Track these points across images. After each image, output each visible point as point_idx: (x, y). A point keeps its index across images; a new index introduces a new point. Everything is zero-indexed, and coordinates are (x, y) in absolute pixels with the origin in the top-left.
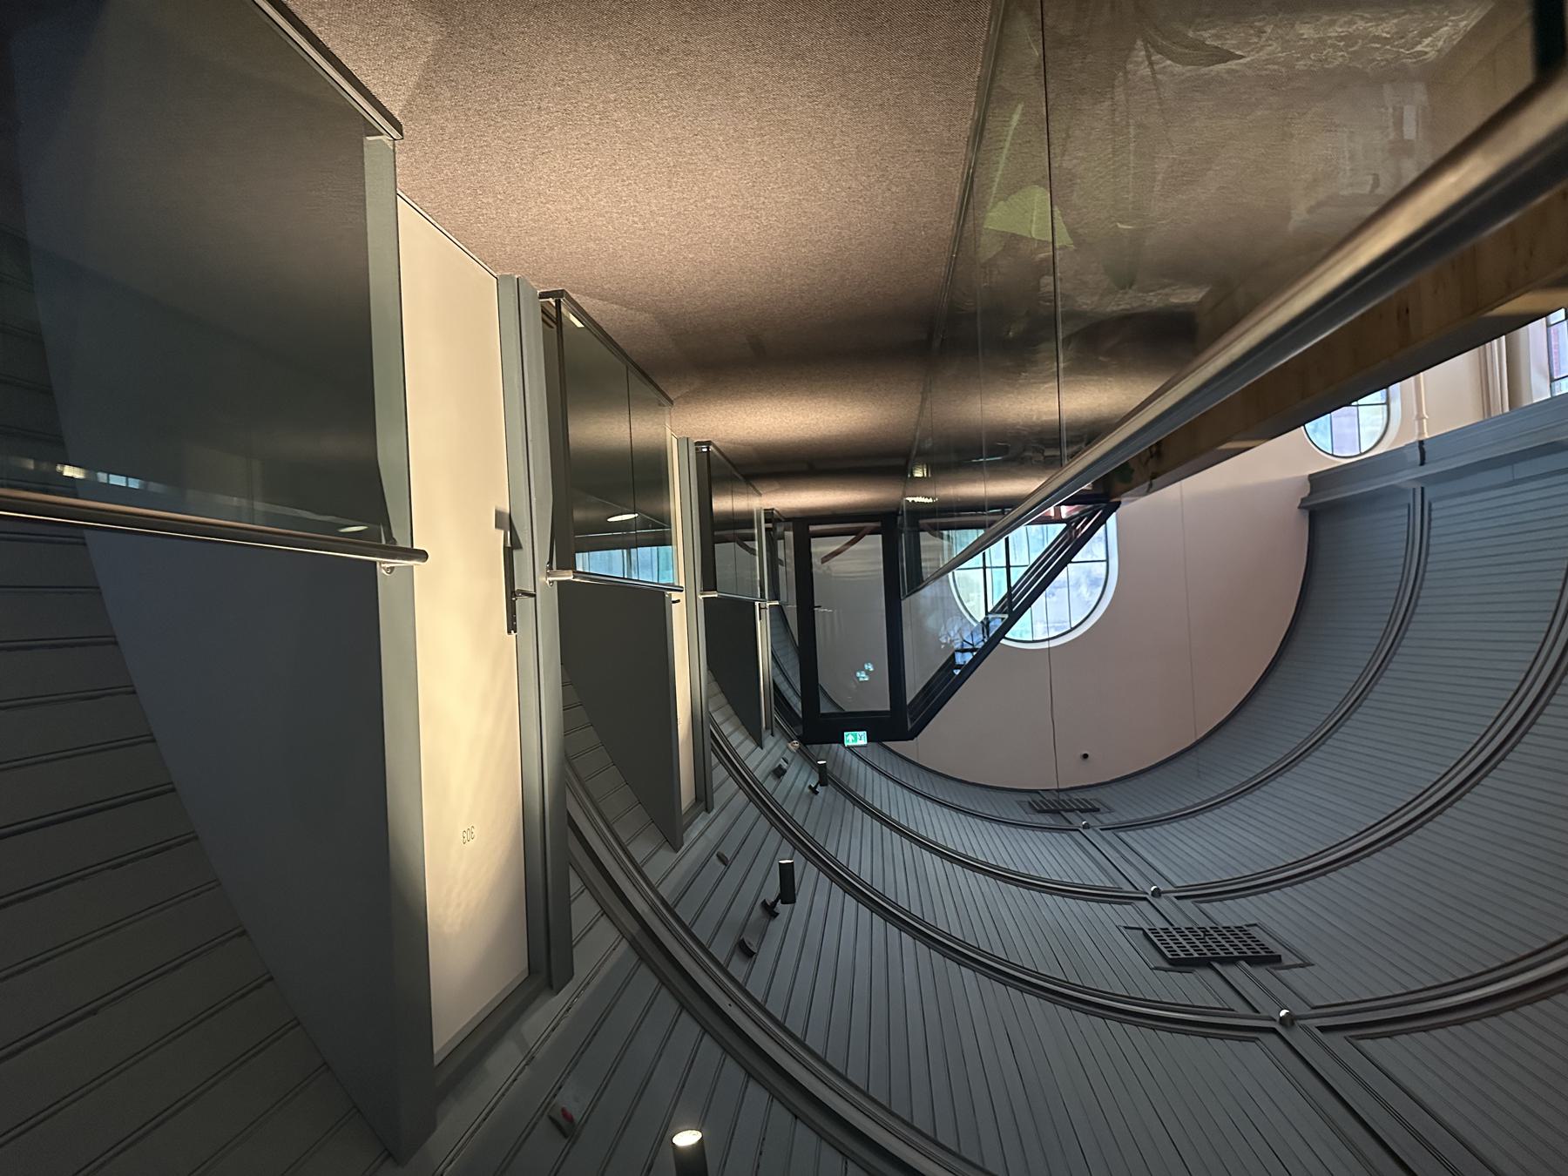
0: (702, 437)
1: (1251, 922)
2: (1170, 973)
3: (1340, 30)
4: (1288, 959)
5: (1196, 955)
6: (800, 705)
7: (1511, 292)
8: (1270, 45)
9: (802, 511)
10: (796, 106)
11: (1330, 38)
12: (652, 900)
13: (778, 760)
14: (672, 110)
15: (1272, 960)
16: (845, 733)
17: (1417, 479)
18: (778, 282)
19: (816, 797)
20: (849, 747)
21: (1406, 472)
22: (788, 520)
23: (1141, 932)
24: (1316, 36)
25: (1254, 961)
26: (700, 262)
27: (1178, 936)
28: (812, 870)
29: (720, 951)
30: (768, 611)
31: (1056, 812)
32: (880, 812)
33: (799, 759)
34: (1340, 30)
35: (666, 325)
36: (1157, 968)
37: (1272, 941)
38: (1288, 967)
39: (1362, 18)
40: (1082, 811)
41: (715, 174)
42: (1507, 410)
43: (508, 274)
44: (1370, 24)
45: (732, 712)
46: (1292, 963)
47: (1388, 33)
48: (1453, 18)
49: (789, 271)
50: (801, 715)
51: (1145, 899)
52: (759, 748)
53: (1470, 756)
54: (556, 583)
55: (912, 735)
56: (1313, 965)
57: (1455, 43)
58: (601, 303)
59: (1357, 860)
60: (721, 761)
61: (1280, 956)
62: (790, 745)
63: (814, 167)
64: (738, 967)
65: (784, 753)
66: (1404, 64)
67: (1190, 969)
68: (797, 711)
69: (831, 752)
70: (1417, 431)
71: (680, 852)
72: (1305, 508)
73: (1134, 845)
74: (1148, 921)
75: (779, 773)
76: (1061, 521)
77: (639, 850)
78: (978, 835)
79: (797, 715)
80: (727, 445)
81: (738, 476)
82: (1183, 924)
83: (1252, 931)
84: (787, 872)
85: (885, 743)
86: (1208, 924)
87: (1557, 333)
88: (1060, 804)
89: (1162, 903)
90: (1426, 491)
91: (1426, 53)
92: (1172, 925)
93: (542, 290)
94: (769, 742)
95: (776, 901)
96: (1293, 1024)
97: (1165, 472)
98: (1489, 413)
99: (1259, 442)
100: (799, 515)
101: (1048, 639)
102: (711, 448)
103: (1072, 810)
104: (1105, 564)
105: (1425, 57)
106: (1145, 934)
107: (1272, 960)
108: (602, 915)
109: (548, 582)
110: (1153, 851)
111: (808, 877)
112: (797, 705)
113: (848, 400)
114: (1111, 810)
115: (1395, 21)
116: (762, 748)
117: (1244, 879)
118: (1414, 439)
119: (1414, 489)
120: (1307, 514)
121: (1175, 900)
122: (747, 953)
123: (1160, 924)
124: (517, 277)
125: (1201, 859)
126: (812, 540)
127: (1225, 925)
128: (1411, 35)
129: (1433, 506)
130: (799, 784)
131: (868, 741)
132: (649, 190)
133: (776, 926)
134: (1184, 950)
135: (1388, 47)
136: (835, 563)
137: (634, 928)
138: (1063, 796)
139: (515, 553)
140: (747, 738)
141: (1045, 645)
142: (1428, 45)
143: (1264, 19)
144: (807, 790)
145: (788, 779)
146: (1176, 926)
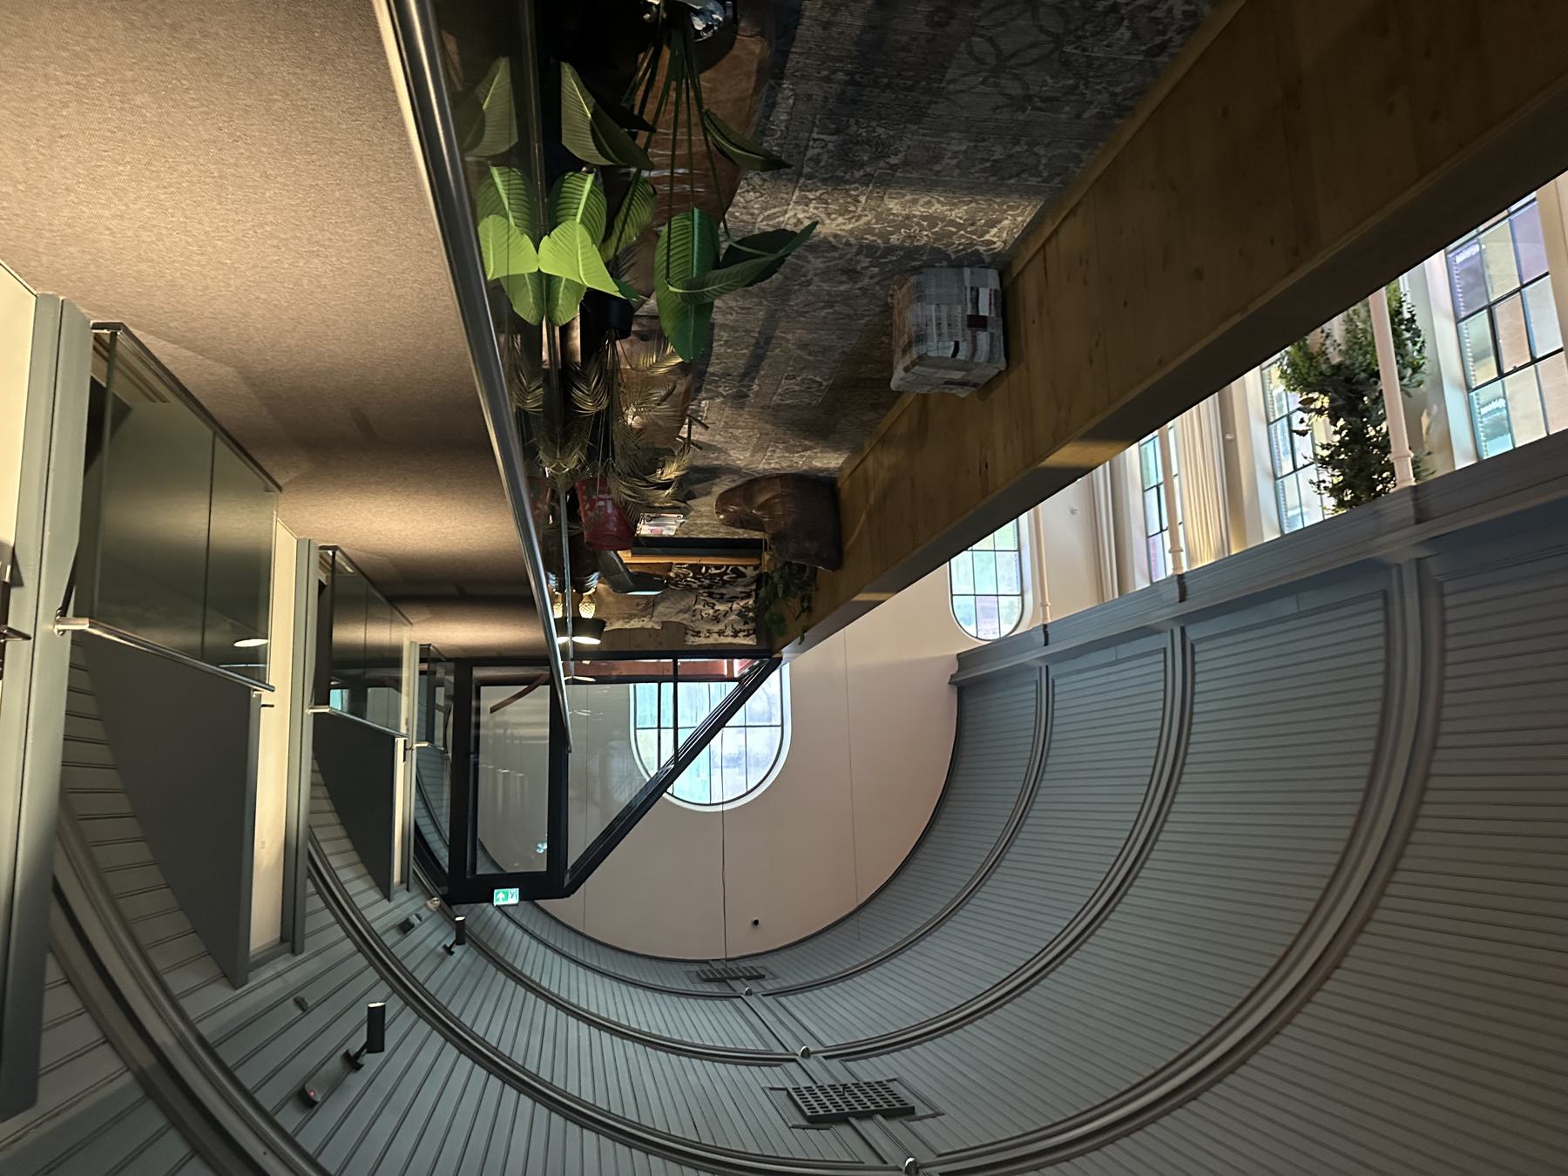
0: (327, 541)
1: (891, 1077)
2: (807, 1131)
3: (923, 210)
4: (921, 1110)
5: (834, 1111)
6: (447, 860)
7: (1057, 443)
8: (866, 215)
9: (465, 649)
10: (339, 123)
11: (915, 216)
12: (182, 1034)
13: (411, 914)
14: (202, 105)
15: (907, 1112)
16: (496, 891)
17: (1041, 658)
18: (368, 343)
19: (449, 957)
20: (498, 907)
21: (1034, 652)
22: (449, 660)
23: (785, 1092)
24: (904, 212)
25: (889, 1114)
26: (276, 306)
27: (819, 1094)
28: (409, 1016)
29: (269, 1098)
30: (415, 752)
31: (722, 980)
32: (558, 997)
33: (438, 918)
34: (923, 210)
35: (254, 385)
36: (794, 1127)
37: (908, 1094)
38: (920, 1119)
39: (939, 202)
40: (749, 978)
41: (267, 195)
42: (1117, 596)
43: (50, 293)
44: (945, 208)
45: (365, 871)
46: (924, 1114)
47: (960, 218)
48: (1010, 212)
49: (378, 331)
50: (447, 870)
51: (794, 1060)
52: (385, 901)
53: (1087, 908)
54: (68, 636)
55: (568, 892)
56: (943, 1114)
57: (1016, 236)
58: (170, 346)
59: (991, 1012)
60: (319, 892)
61: (913, 1108)
62: (429, 903)
63: (374, 202)
64: (290, 1118)
65: (421, 908)
66: (977, 251)
67: (826, 1125)
68: (443, 865)
69: (483, 917)
70: (1041, 616)
71: (238, 992)
72: (955, 683)
73: (792, 1009)
74: (793, 1080)
75: (406, 927)
76: (734, 680)
77: (178, 982)
78: (636, 1003)
79: (444, 871)
80: (359, 553)
81: (379, 596)
82: (826, 1081)
83: (891, 1086)
84: (376, 1020)
85: (539, 902)
86: (849, 1080)
87: (1154, 544)
88: (726, 972)
89: (810, 1064)
90: (1050, 668)
91: (995, 243)
92: (815, 1083)
93: (96, 321)
94: (401, 896)
95: (362, 1050)
96: (917, 1172)
97: (813, 626)
98: (1103, 600)
99: (888, 595)
100: (463, 655)
101: (723, 803)
102: (338, 553)
103: (738, 978)
104: (780, 728)
105: (993, 246)
106: (789, 1093)
107: (907, 1112)
108: (104, 1043)
109: (56, 631)
110: (810, 1014)
111: (402, 1024)
112: (443, 855)
113: (482, 506)
114: (775, 977)
115: (965, 208)
116: (389, 901)
117: (890, 1036)
118: (1039, 623)
119: (1041, 668)
120: (956, 690)
121: (823, 1060)
122: (305, 1101)
123: (804, 1082)
124: (61, 298)
125: (852, 1019)
126: (483, 689)
127: (866, 1080)
128: (979, 223)
129: (1056, 683)
130: (432, 942)
131: (521, 899)
132: (199, 204)
133: (357, 1081)
134: (823, 1106)
135: (962, 232)
136: (499, 716)
137: (146, 1059)
138: (730, 965)
139: (14, 591)
140: (371, 888)
141: (719, 808)
142: (994, 236)
143: (857, 189)
144: (440, 949)
145: (415, 936)
146: (820, 1084)
